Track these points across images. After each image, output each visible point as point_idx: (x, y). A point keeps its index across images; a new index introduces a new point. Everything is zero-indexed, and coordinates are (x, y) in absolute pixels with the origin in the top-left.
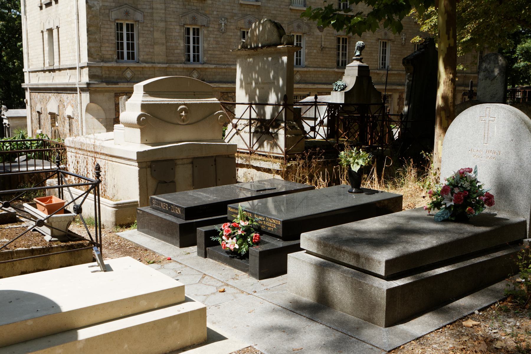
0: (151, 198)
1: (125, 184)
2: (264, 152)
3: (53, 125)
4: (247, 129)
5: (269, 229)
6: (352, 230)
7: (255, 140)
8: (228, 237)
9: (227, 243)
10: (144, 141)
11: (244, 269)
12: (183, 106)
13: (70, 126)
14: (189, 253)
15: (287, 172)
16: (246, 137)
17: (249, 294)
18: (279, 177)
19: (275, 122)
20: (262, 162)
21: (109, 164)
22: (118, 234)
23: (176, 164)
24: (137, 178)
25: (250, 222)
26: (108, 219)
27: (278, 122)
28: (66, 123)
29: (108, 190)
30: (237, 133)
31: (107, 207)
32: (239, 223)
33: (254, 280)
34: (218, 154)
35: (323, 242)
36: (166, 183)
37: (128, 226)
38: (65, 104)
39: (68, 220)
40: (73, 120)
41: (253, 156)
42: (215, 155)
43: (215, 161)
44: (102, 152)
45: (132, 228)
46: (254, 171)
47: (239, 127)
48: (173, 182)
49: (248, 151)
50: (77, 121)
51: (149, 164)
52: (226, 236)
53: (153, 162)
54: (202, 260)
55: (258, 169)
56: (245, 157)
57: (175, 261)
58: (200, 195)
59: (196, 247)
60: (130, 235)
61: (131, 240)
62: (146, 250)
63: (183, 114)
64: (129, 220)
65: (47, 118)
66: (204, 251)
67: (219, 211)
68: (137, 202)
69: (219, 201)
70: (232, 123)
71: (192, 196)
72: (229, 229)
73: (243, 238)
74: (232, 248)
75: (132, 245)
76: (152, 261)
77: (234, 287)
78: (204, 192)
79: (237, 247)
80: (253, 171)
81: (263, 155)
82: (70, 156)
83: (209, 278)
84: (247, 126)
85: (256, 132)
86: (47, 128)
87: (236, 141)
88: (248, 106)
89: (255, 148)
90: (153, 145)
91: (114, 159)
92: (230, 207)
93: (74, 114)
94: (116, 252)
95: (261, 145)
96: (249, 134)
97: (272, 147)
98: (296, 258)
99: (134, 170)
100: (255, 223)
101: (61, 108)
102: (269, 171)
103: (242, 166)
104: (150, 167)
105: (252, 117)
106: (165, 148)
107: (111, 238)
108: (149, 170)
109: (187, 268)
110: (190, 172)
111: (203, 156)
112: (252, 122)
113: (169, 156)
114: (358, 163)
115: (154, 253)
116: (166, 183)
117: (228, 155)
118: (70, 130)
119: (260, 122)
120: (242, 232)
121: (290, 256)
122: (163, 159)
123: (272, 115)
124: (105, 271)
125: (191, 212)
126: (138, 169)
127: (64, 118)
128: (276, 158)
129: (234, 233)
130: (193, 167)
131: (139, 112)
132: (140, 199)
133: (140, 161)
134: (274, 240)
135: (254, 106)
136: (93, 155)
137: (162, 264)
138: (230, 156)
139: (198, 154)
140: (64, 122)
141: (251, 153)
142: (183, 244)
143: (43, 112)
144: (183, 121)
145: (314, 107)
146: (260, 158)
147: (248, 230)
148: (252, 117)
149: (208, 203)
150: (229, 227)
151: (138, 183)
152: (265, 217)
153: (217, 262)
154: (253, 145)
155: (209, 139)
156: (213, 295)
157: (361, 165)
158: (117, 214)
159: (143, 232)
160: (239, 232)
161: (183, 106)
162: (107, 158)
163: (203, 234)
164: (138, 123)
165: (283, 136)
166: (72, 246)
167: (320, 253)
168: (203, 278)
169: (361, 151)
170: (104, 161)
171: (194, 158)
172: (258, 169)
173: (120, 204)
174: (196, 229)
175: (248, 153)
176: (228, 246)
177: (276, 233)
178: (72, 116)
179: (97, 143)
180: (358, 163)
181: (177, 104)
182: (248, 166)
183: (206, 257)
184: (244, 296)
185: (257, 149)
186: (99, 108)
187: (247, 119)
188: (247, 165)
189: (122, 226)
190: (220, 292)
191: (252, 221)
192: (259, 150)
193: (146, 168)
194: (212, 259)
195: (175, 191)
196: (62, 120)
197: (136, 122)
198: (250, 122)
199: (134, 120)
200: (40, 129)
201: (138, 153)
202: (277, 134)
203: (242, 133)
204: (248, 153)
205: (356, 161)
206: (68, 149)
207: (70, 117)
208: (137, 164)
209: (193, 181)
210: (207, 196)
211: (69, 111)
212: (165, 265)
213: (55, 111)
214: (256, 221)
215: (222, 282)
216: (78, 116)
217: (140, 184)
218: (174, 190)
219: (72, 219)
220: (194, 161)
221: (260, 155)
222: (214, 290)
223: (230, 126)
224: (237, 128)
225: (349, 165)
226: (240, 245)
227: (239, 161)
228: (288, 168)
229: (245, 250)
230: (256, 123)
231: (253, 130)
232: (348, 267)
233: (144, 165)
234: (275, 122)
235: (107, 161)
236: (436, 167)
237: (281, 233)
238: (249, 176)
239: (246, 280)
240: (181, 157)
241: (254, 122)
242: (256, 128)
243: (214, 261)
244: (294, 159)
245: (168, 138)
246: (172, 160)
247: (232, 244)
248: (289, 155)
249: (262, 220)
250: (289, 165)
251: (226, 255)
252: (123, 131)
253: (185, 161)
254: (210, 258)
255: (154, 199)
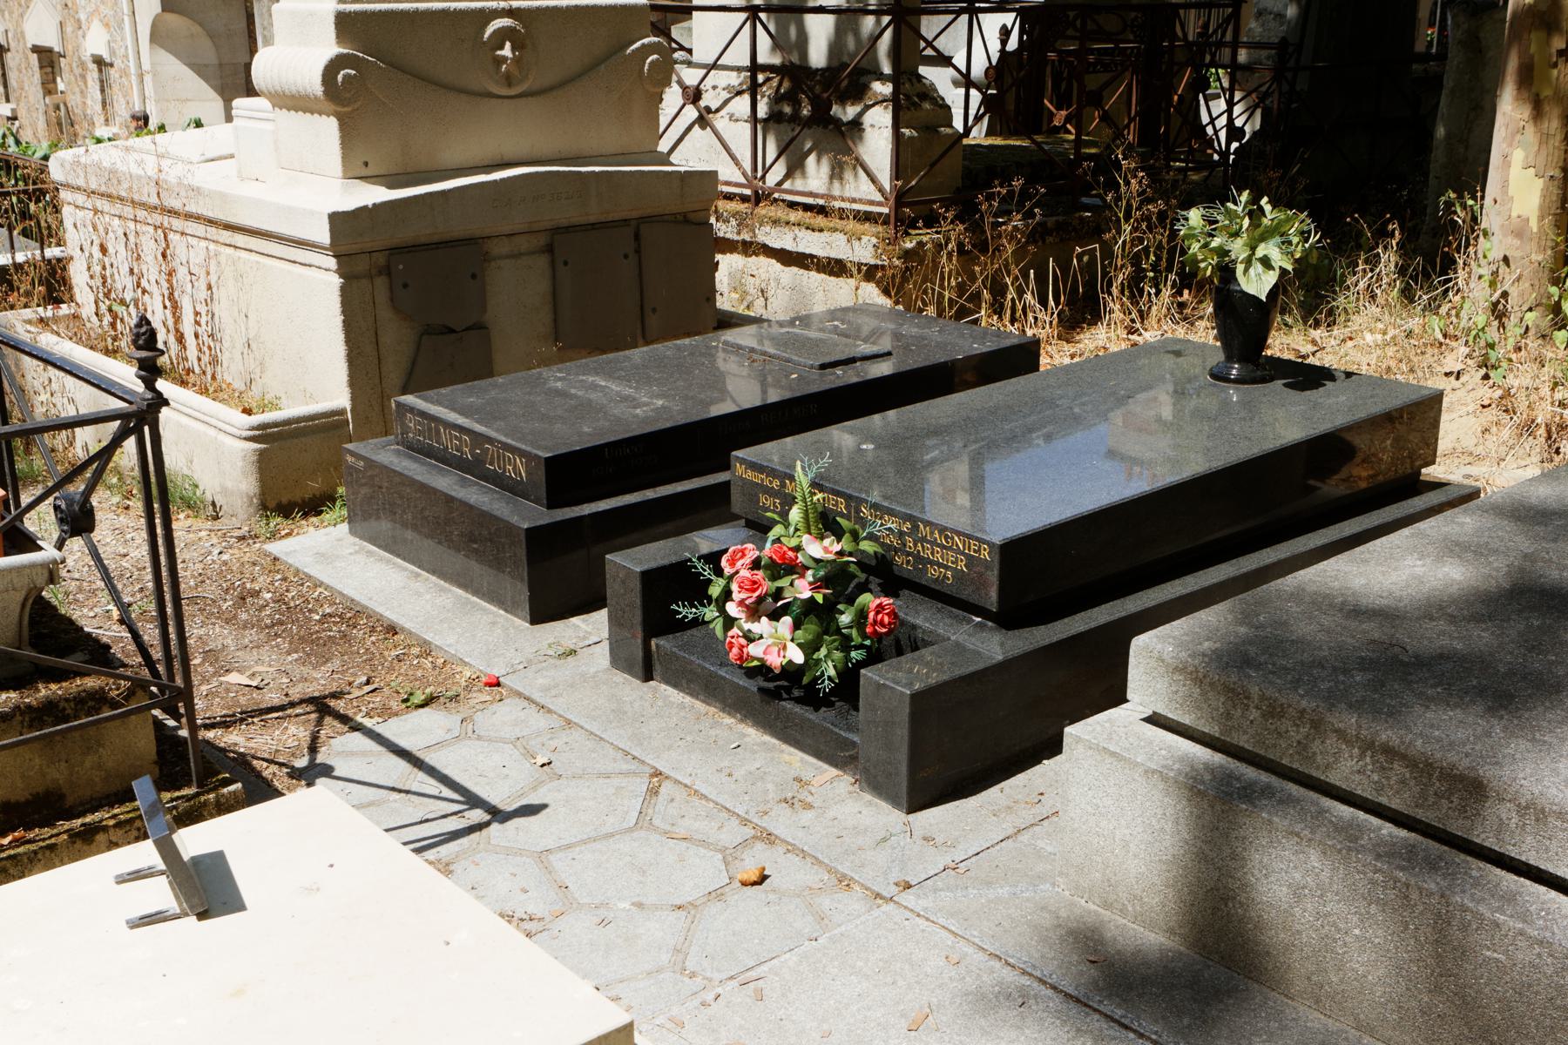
0: (398, 404)
1: (294, 344)
2: (811, 194)
3: (49, 87)
4: (742, 105)
5: (933, 572)
6: (1357, 612)
7: (772, 152)
8: (754, 612)
9: (750, 638)
10: (357, 168)
11: (837, 753)
12: (505, 22)
13: (102, 91)
14: (573, 652)
15: (906, 274)
16: (739, 136)
17: (878, 896)
18: (871, 293)
19: (847, 78)
20: (803, 234)
21: (223, 259)
22: (275, 548)
23: (486, 258)
24: (338, 320)
25: (845, 544)
26: (229, 484)
27: (863, 79)
28: (90, 83)
29: (225, 358)
30: (702, 121)
31: (222, 436)
32: (798, 549)
33: (882, 815)
34: (649, 212)
35: (1228, 674)
36: (452, 331)
37: (313, 507)
38: (82, 17)
39: (23, 583)
40: (112, 71)
41: (764, 210)
42: (635, 214)
43: (637, 237)
44: (192, 208)
45: (326, 517)
46: (774, 265)
47: (709, 99)
48: (480, 327)
49: (748, 192)
50: (125, 73)
51: (381, 259)
52: (741, 603)
53: (396, 251)
54: (630, 688)
55: (788, 258)
56: (735, 215)
57: (519, 695)
58: (594, 387)
59: (601, 616)
60: (322, 557)
61: (326, 581)
62: (392, 630)
63: (507, 51)
64: (315, 486)
65: (28, 66)
66: (640, 654)
67: (689, 465)
68: (342, 412)
69: (681, 420)
70: (680, 82)
71: (562, 394)
72: (760, 575)
73: (816, 615)
74: (775, 661)
75: (333, 603)
76: (419, 698)
77: (804, 854)
78: (610, 375)
79: (798, 657)
80: (766, 267)
81: (807, 208)
82: (74, 217)
83: (680, 794)
84: (739, 93)
85: (775, 118)
86: (31, 99)
87: (694, 154)
88: (743, 16)
89: (772, 179)
90: (392, 182)
91: (240, 239)
92: (743, 461)
93: (112, 52)
94: (269, 638)
95: (795, 167)
96: (748, 126)
97: (837, 173)
98: (1113, 754)
99: (319, 290)
100: (867, 546)
101: (69, 29)
102: (836, 268)
103: (728, 246)
104: (387, 271)
105: (761, 60)
106: (443, 193)
107: (248, 569)
108: (381, 282)
109: (576, 734)
110: (544, 286)
111: (592, 219)
112: (761, 78)
113: (458, 227)
114: (1266, 263)
115: (427, 650)
116: (452, 331)
117: (685, 215)
118: (104, 103)
119: (792, 80)
120: (815, 586)
121: (1078, 740)
122: (436, 239)
123: (835, 48)
124: (203, 916)
125: (569, 474)
126: (336, 281)
127: (82, 64)
128: (868, 217)
129: (778, 594)
130: (553, 264)
131: (331, 48)
132: (353, 399)
133: (343, 250)
134: (961, 621)
135: (763, 16)
136: (157, 218)
137: (464, 710)
138: (691, 216)
139: (570, 214)
140: (83, 77)
141: (758, 198)
142: (547, 607)
143: (13, 45)
144: (509, 80)
145: (965, 18)
146: (794, 216)
147: (838, 580)
148: (761, 60)
149: (637, 431)
150: (756, 564)
151: (338, 300)
152: (912, 519)
153: (698, 705)
154: (766, 171)
155: (612, 150)
156: (715, 907)
157: (1283, 271)
158: (264, 465)
159: (373, 540)
160: (802, 589)
161: (505, 22)
162: (212, 232)
163: (636, 585)
164: (326, 92)
165: (887, 133)
166: (50, 711)
167: (1211, 729)
168: (653, 792)
169: (1268, 208)
170: (203, 244)
171: (557, 231)
172: (788, 258)
173: (276, 424)
174: (602, 563)
175: (744, 199)
176: (755, 650)
177: (966, 594)
178: (107, 58)
179: (172, 174)
180: (1266, 263)
181: (482, 10)
182: (749, 248)
183: (648, 676)
184: (853, 902)
185: (780, 184)
186: (197, 29)
187: (739, 69)
188: (744, 242)
189: (286, 511)
190: (744, 884)
191: (855, 537)
192: (786, 185)
193: (371, 277)
194: (675, 686)
195: (491, 374)
196: (78, 71)
197: (317, 88)
198: (754, 78)
199: (313, 83)
200: (8, 100)
201: (336, 219)
202: (856, 125)
203: (720, 122)
204: (744, 199)
205: (1260, 252)
206: (64, 195)
207: (99, 62)
208: (332, 263)
209: (555, 320)
210: (623, 395)
211: (95, 42)
212: (479, 717)
213: (51, 40)
214: (872, 537)
215: (745, 822)
216: (126, 56)
217: (348, 341)
218: (483, 369)
219: (41, 579)
220: (558, 243)
221: (792, 205)
222: (706, 871)
223: (672, 98)
224: (702, 103)
225: (1226, 271)
226: (809, 648)
227: (725, 230)
228: (907, 255)
229: (832, 672)
230: (775, 83)
231: (762, 111)
232: (1367, 811)
233: (362, 265)
234: (847, 78)
235: (212, 246)
236: (1496, 255)
237: (993, 594)
238: (751, 285)
239: (842, 810)
240: (507, 229)
241: (768, 80)
242: (777, 99)
243: (688, 699)
244: (931, 221)
245: (454, 153)
246: (470, 241)
247: (777, 644)
248: (908, 209)
249: (901, 534)
250: (909, 245)
251: (743, 682)
252: (269, 126)
253: (523, 243)
254: (668, 682)
255: (412, 410)
